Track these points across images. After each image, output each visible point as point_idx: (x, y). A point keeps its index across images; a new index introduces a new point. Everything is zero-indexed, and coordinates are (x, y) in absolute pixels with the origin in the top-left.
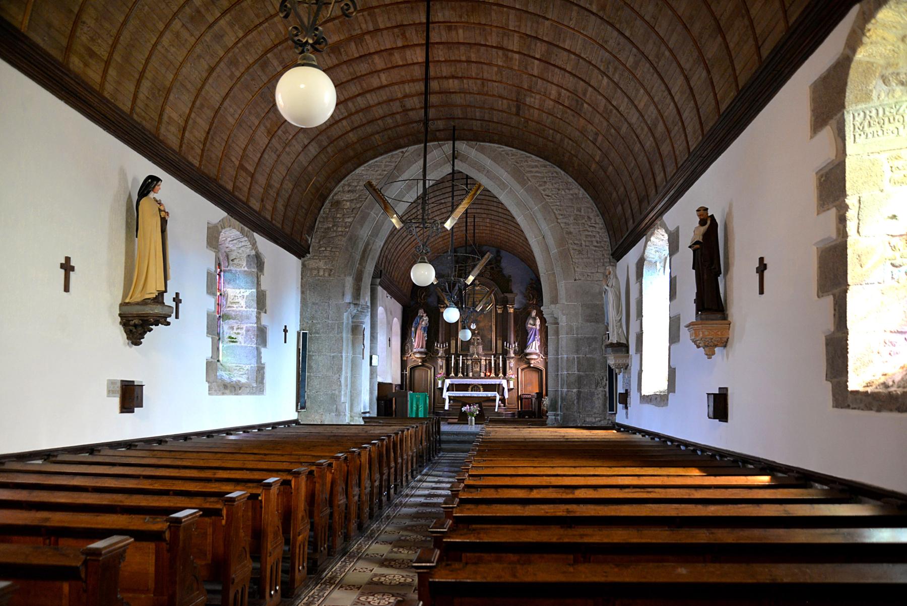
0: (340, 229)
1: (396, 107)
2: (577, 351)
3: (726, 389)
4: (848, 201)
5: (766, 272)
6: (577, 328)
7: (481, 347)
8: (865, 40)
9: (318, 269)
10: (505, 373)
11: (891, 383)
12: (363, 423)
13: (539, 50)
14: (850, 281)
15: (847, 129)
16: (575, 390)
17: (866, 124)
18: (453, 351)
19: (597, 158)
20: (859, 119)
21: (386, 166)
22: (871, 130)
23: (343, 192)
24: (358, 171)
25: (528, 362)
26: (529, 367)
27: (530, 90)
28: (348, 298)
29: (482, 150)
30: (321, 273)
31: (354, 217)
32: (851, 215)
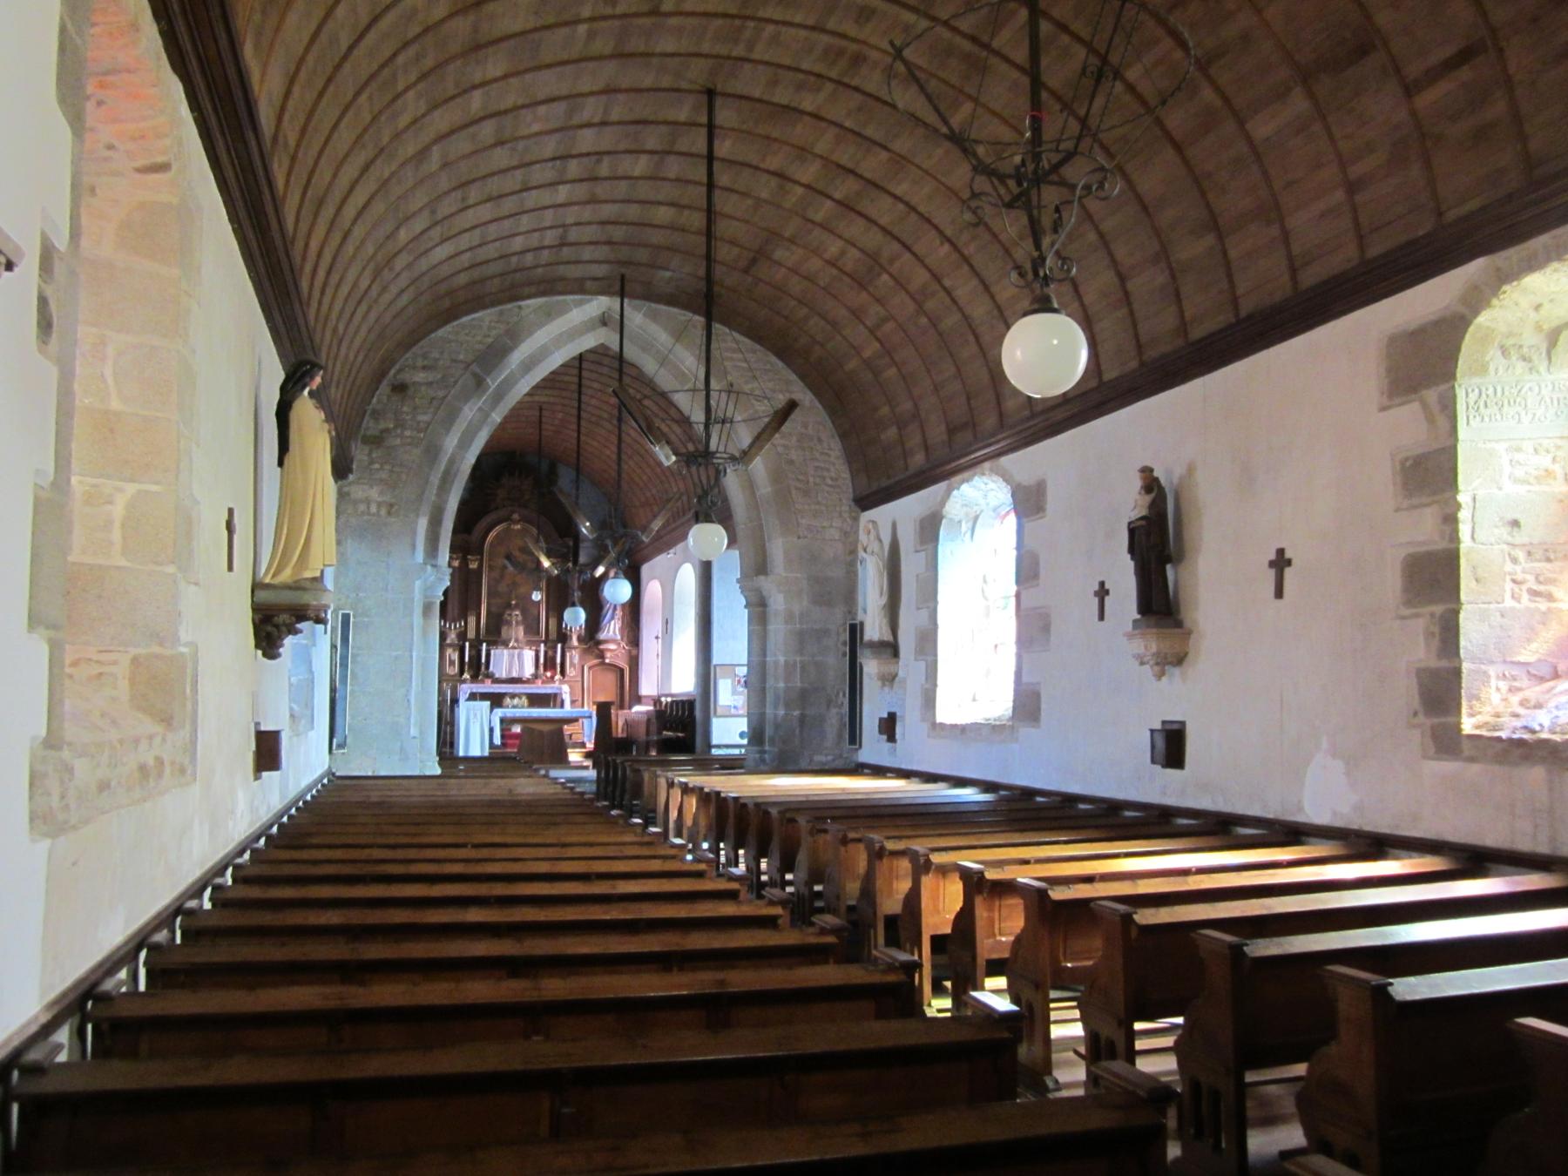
0: (408, 433)
1: (550, 237)
2: (801, 651)
3: (1183, 723)
4: (1461, 498)
5: (1288, 572)
6: (802, 615)
7: (521, 629)
8: (1495, 302)
9: (368, 502)
10: (563, 673)
11: (1538, 728)
12: (438, 771)
13: (844, 188)
14: (1463, 597)
15: (1458, 407)
16: (796, 713)
17: (1482, 404)
18: (471, 634)
19: (867, 354)
20: (1473, 397)
21: (490, 328)
22: (1488, 411)
23: (414, 368)
24: (441, 332)
25: (601, 655)
26: (603, 663)
27: (792, 241)
28: (420, 556)
29: (654, 316)
30: (373, 509)
31: (435, 414)
32: (1463, 515)
